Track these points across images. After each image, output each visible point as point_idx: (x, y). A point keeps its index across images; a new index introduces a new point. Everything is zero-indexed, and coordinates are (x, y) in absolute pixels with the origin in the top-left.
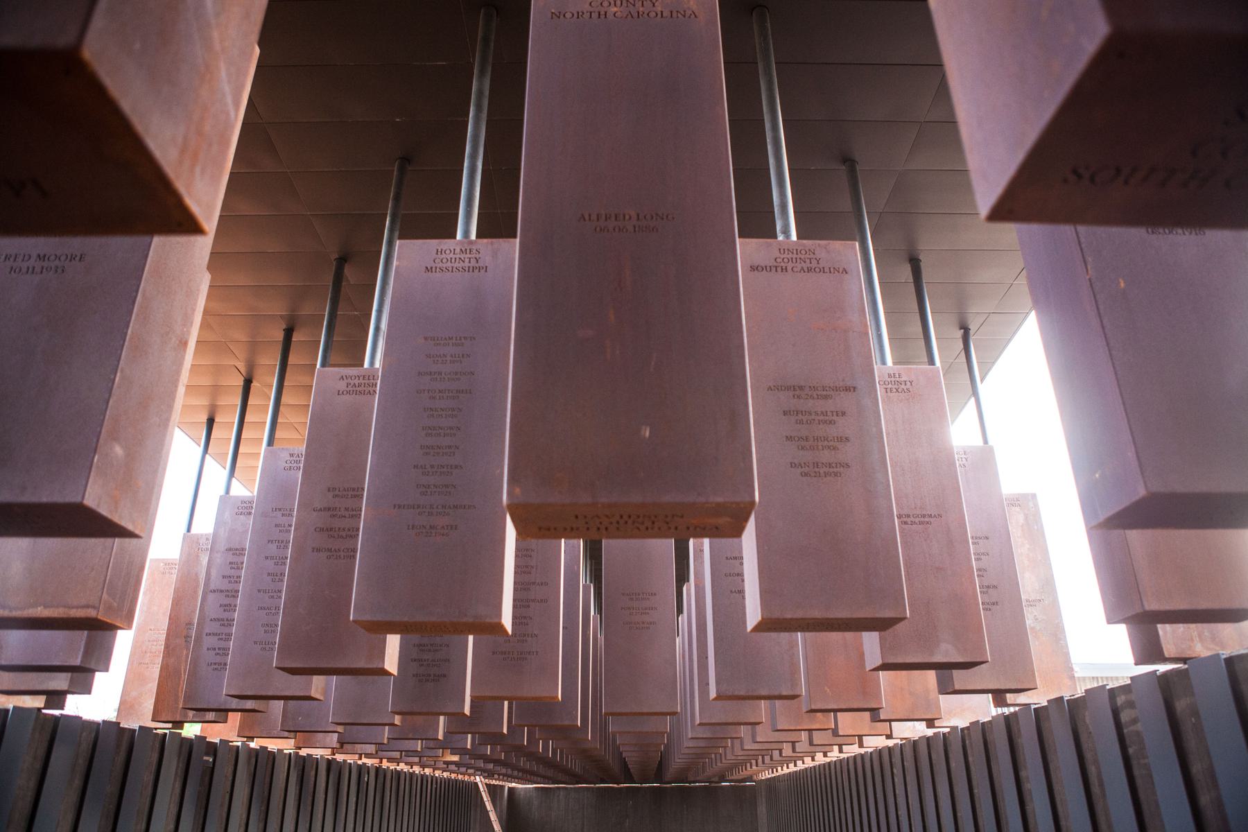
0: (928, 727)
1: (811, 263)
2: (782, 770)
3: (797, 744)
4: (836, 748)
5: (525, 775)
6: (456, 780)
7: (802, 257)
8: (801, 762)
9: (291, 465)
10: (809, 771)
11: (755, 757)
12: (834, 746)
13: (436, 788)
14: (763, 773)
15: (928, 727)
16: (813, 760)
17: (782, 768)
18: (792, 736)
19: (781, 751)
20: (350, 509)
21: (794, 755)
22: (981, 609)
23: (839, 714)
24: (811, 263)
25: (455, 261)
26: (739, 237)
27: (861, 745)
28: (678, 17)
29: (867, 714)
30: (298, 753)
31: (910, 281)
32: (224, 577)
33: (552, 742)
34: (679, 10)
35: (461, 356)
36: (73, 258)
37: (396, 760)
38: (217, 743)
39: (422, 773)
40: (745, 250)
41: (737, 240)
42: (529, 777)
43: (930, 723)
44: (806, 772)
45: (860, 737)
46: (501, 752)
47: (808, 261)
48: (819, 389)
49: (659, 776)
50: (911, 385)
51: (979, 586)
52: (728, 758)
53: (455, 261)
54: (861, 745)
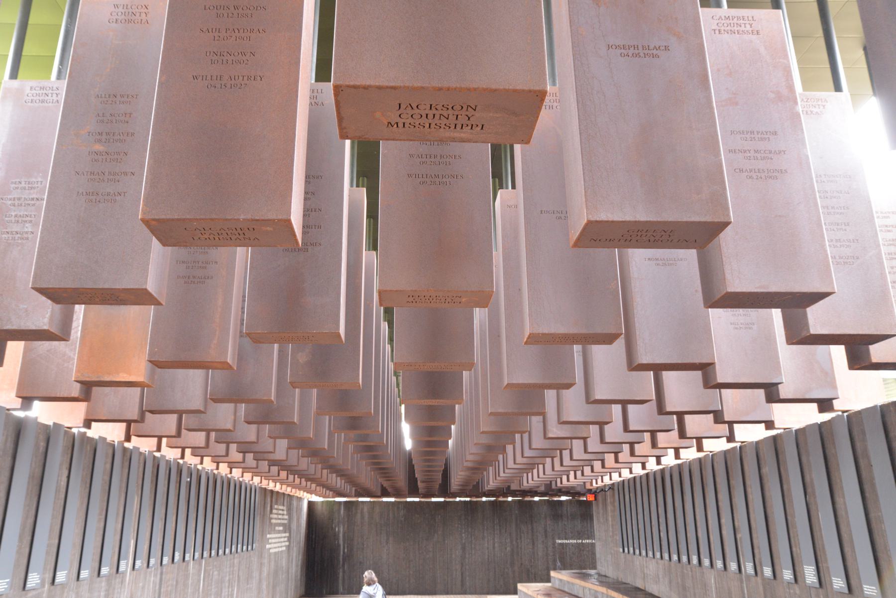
1: (745, 27)
2: (597, 483)
6: (241, 483)
10: (626, 484)
11: (596, 478)
13: (190, 484)
14: (530, 475)
17: (596, 480)
18: (582, 431)
19: (603, 461)
20: (659, 259)
22: (890, 287)
24: (745, 27)
30: (85, 433)
32: (178, 277)
33: (337, 435)
35: (107, 96)
36: (249, 78)
37: (260, 474)
38: (50, 426)
39: (251, 482)
42: (297, 481)
44: (623, 485)
45: (653, 433)
46: (371, 471)
47: (743, 25)
48: (36, 89)
49: (444, 490)
51: (831, 257)
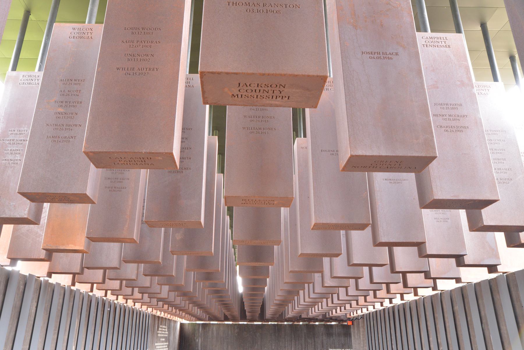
0: (490, 272)
3: (377, 292)
4: (398, 296)
5: (170, 308)
7: (434, 44)
8: (366, 309)
9: (24, 82)
12: (386, 300)
15: (490, 272)
16: (382, 305)
19: (357, 301)
21: (351, 309)
23: (340, 288)
25: (29, 80)
26: (417, 32)
27: (416, 294)
28: (129, 56)
29: (453, 260)
31: (515, 50)
34: (297, 4)
40: (419, 35)
41: (416, 32)
42: (174, 311)
43: (492, 269)
50: (489, 91)
52: (296, 309)
53: (29, 80)
54: (416, 294)
